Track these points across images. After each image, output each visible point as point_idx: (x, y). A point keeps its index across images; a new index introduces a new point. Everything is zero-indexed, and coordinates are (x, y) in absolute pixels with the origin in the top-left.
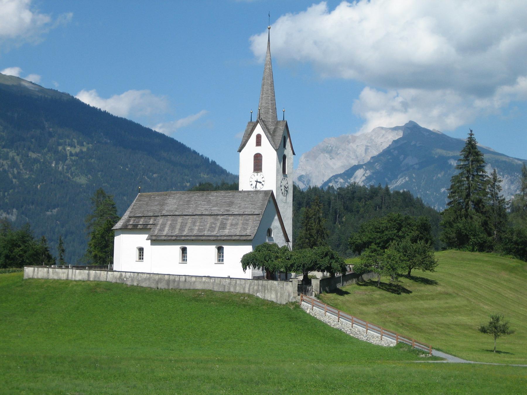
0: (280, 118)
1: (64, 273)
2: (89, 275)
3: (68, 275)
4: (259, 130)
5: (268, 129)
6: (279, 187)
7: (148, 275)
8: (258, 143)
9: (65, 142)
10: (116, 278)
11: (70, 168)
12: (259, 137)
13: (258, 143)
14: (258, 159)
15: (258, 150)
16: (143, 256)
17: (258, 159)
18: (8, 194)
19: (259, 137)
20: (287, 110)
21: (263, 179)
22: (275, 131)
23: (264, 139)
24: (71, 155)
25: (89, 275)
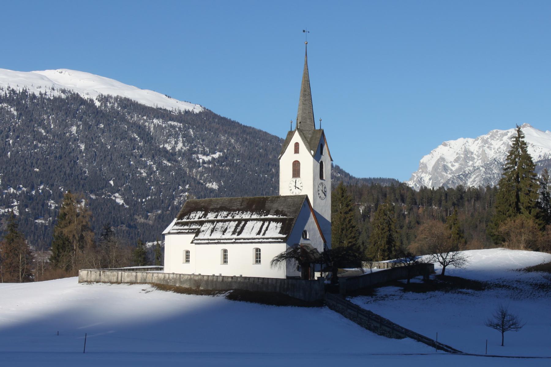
0: (317, 128)
1: (114, 276)
2: (136, 276)
3: (117, 278)
4: (297, 138)
5: (305, 138)
6: (316, 192)
7: (103, 278)
8: (297, 151)
9: (198, 151)
10: (160, 280)
11: (203, 175)
12: (297, 145)
13: (297, 151)
14: (296, 166)
15: (296, 157)
16: (260, 258)
17: (296, 166)
18: (146, 200)
19: (297, 145)
20: (323, 119)
21: (301, 185)
22: (311, 139)
23: (303, 147)
24: (204, 162)
25: (136, 276)
